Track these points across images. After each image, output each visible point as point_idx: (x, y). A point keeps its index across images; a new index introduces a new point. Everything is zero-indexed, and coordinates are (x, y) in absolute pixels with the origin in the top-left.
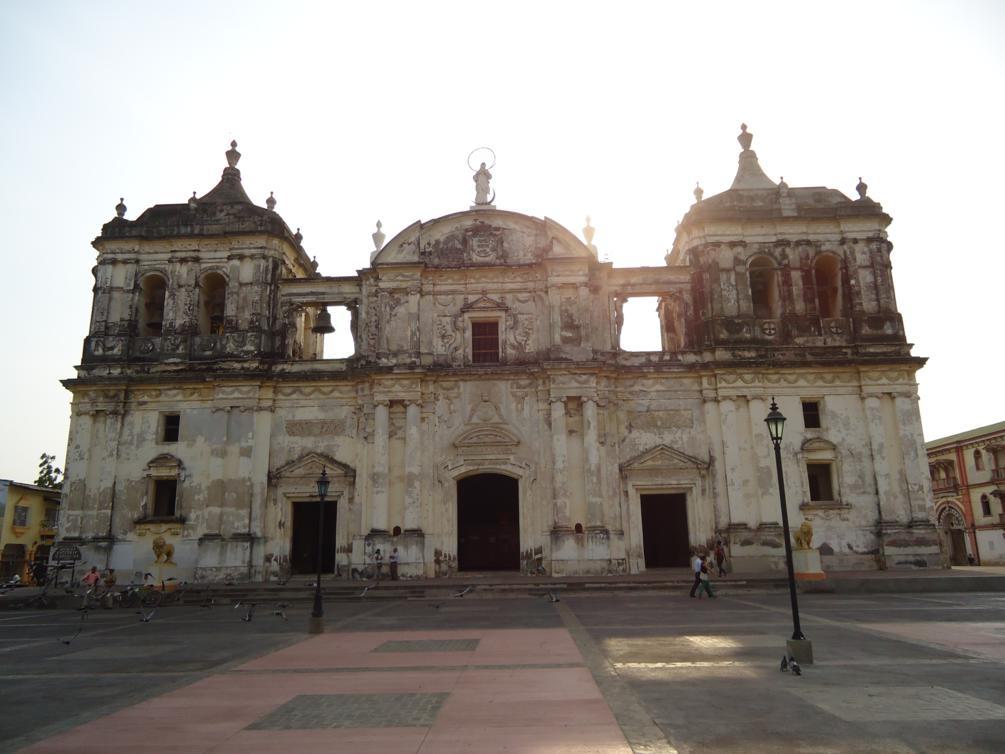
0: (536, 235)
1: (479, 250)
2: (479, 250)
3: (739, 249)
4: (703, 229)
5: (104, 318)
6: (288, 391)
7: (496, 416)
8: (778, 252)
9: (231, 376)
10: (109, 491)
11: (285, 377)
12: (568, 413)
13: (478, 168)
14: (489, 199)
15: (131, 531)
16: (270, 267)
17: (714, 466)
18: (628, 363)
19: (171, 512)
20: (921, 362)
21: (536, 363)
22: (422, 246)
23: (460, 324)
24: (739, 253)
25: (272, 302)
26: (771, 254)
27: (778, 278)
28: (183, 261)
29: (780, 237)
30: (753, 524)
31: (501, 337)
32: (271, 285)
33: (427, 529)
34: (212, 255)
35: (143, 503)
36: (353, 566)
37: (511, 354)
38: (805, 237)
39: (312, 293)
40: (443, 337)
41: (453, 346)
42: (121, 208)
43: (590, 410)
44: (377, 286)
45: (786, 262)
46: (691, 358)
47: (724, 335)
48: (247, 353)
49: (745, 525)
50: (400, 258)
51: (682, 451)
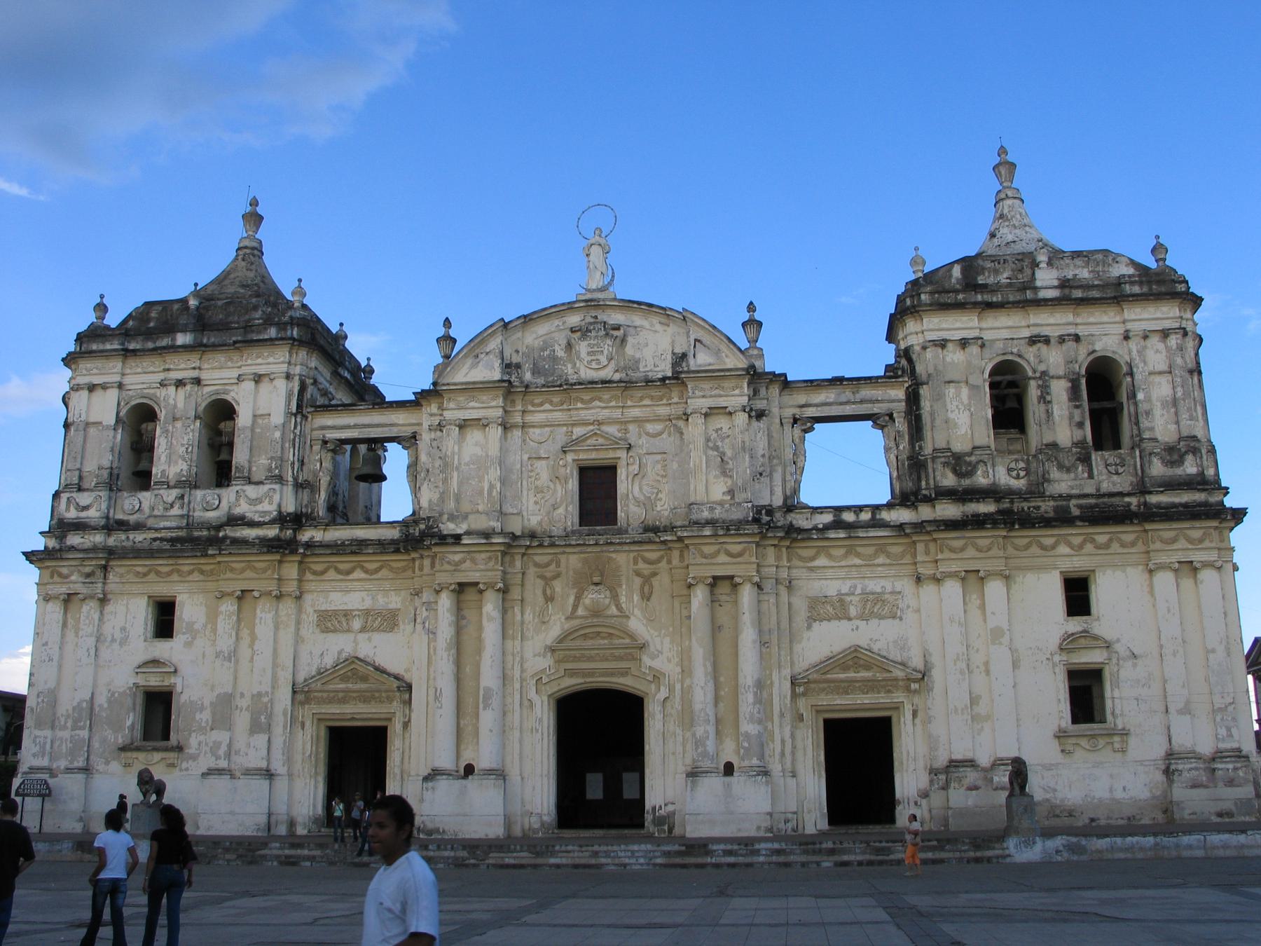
1: (590, 358)
2: (590, 358)
5: (78, 466)
6: (318, 568)
7: (614, 608)
10: (84, 705)
15: (114, 759)
17: (930, 676)
18: (806, 524)
19: (166, 736)
20: (1238, 515)
25: (299, 442)
28: (180, 383)
29: (1036, 331)
30: (984, 760)
31: (622, 487)
32: (295, 415)
35: (129, 723)
38: (1072, 330)
39: (355, 426)
42: (101, 308)
43: (747, 594)
44: (441, 415)
45: (1042, 368)
46: (903, 515)
47: (949, 480)
49: (971, 761)
51: (884, 654)
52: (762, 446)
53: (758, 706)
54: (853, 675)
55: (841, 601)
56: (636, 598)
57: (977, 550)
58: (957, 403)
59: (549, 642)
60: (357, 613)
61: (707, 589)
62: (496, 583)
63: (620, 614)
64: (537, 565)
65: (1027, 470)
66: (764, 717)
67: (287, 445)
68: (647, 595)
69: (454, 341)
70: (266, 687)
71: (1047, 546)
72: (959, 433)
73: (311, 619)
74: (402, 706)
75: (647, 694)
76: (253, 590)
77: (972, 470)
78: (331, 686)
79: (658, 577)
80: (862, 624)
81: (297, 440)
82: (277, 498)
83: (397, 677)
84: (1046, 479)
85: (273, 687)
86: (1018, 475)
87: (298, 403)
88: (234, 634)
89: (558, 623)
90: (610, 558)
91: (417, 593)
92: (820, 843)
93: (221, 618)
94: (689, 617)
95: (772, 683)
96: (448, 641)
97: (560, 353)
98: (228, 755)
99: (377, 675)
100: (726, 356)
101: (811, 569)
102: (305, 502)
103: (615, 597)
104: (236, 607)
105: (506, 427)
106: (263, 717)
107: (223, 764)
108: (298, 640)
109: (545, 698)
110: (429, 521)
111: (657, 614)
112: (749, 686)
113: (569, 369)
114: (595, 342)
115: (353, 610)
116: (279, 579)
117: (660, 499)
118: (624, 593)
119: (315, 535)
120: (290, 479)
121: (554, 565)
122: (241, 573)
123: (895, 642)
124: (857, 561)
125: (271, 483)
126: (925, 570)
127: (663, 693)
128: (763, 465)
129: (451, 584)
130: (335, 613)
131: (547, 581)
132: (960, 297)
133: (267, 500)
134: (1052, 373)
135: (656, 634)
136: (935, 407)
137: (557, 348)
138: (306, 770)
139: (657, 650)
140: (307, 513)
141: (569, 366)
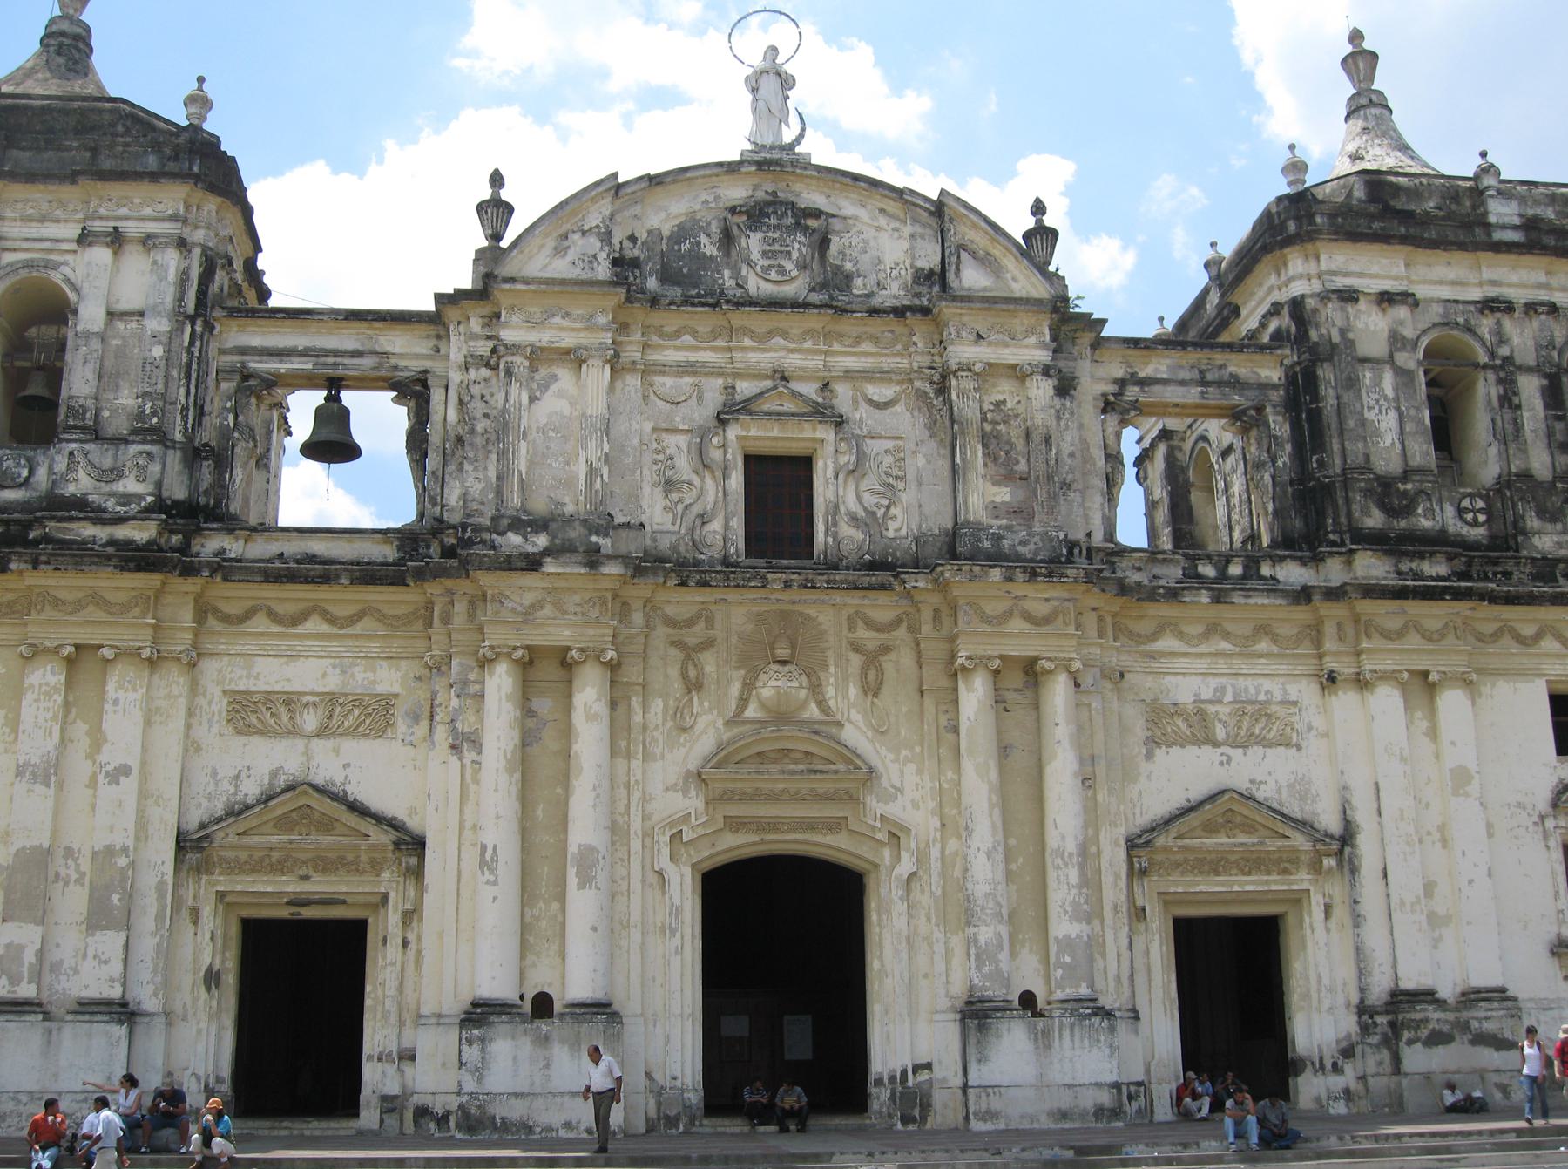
0: (912, 236)
1: (766, 263)
2: (766, 263)
3: (1402, 312)
4: (1318, 258)
7: (813, 706)
8: (1486, 325)
9: (80, 555)
11: (224, 568)
12: (1000, 702)
13: (756, 59)
14: (788, 136)
16: (195, 274)
17: (1353, 846)
21: (918, 564)
22: (616, 241)
23: (716, 455)
24: (1402, 323)
25: (194, 369)
26: (1470, 330)
27: (1486, 389)
29: (1492, 292)
30: (1446, 992)
31: (823, 491)
32: (192, 319)
33: (628, 1004)
34: (34, 230)
36: (416, 1100)
37: (851, 539)
38: (1543, 296)
40: (669, 485)
41: (696, 509)
43: (1058, 693)
45: (1504, 351)
46: (1292, 573)
47: (1374, 520)
48: (126, 499)
49: (1503, 990)
50: (561, 268)
52: (1069, 439)
53: (1085, 890)
54: (1225, 840)
55: (1201, 713)
56: (853, 691)
57: (1423, 636)
58: (1377, 396)
59: (693, 765)
60: (310, 698)
61: (989, 677)
62: (603, 650)
63: (823, 718)
64: (671, 622)
65: (1488, 511)
66: (1091, 912)
67: (175, 373)
68: (872, 684)
69: (509, 209)
70: (123, 837)
71: (1526, 638)
72: (1381, 445)
73: (215, 708)
74: (401, 880)
75: (876, 866)
76: (101, 646)
77: (1407, 506)
78: (257, 839)
79: (893, 656)
80: (1237, 754)
81: (194, 366)
82: (155, 468)
83: (393, 824)
84: (1520, 530)
85: (137, 839)
86: (1475, 519)
87: (197, 298)
88: (56, 729)
89: (712, 731)
90: (808, 617)
91: (440, 666)
92: (1318, 1140)
93: (28, 699)
94: (955, 730)
95: (1099, 853)
96: (509, 756)
97: (709, 248)
98: (37, 975)
99: (352, 820)
100: (1014, 279)
101: (1152, 656)
102: (205, 485)
103: (816, 689)
104: (63, 678)
105: (617, 366)
106: (115, 898)
107: (27, 991)
108: (191, 747)
109: (687, 871)
110: (464, 530)
111: (893, 719)
112: (1071, 854)
113: (727, 279)
114: (776, 235)
115: (306, 694)
116: (155, 627)
117: (894, 518)
118: (832, 680)
119: (226, 545)
120: (178, 437)
121: (702, 624)
122: (76, 611)
123: (1290, 786)
124: (1224, 645)
125: (144, 442)
126: (1345, 668)
127: (906, 865)
128: (1071, 471)
129: (515, 648)
130: (268, 698)
131: (690, 653)
132: (1376, 225)
133: (134, 472)
134: (1518, 361)
135: (891, 756)
136: (1345, 399)
137: (704, 239)
138: (201, 1003)
139: (893, 786)
140: (207, 505)
141: (727, 273)
